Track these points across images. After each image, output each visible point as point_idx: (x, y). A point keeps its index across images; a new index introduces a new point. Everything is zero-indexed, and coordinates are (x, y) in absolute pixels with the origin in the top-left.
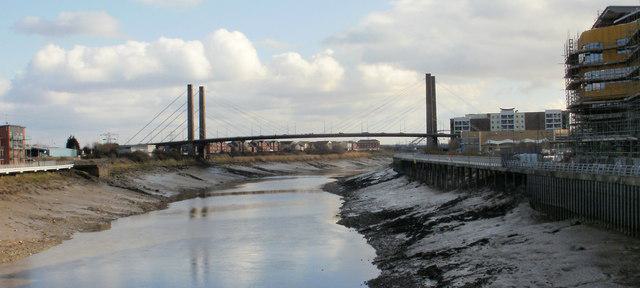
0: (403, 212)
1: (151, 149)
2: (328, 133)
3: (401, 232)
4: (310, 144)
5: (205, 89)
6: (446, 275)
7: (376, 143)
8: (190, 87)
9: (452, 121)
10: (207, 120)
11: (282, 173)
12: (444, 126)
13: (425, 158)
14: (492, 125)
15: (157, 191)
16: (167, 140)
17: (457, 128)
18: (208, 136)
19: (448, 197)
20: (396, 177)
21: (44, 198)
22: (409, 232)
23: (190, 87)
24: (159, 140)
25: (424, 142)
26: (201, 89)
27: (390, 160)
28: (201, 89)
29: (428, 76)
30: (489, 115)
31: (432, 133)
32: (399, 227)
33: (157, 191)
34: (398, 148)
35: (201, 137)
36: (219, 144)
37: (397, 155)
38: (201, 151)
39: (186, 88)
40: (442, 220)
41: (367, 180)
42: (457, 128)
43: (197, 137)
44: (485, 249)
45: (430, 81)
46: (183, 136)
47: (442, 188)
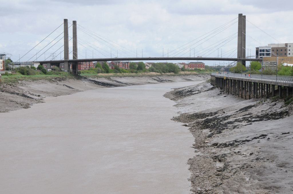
0: (211, 114)
1: (36, 66)
2: (220, 57)
3: (207, 128)
4: (154, 64)
5: (77, 23)
6: (228, 159)
7: (202, 65)
8: (66, 21)
9: (257, 48)
10: (79, 46)
11: (126, 84)
12: (250, 53)
13: (232, 76)
14: (288, 52)
15: (39, 96)
16: (49, 60)
17: (261, 55)
18: (80, 57)
19: (244, 104)
20: (212, 89)
21: (45, 90)
22: (212, 128)
23: (66, 21)
24: (42, 59)
25: (234, 64)
26: (74, 23)
27: (209, 78)
28: (74, 23)
29: (240, 16)
30: (286, 45)
31: (241, 59)
32: (206, 125)
33: (39, 96)
34: (218, 69)
35: (74, 57)
36: (88, 63)
37: (213, 74)
38: (74, 68)
39: (63, 22)
40: (236, 121)
41: (191, 91)
42: (261, 55)
43: (71, 57)
44: (263, 141)
45: (242, 19)
46: (60, 57)
47: (243, 97)
